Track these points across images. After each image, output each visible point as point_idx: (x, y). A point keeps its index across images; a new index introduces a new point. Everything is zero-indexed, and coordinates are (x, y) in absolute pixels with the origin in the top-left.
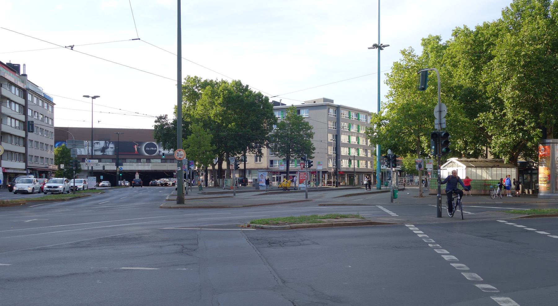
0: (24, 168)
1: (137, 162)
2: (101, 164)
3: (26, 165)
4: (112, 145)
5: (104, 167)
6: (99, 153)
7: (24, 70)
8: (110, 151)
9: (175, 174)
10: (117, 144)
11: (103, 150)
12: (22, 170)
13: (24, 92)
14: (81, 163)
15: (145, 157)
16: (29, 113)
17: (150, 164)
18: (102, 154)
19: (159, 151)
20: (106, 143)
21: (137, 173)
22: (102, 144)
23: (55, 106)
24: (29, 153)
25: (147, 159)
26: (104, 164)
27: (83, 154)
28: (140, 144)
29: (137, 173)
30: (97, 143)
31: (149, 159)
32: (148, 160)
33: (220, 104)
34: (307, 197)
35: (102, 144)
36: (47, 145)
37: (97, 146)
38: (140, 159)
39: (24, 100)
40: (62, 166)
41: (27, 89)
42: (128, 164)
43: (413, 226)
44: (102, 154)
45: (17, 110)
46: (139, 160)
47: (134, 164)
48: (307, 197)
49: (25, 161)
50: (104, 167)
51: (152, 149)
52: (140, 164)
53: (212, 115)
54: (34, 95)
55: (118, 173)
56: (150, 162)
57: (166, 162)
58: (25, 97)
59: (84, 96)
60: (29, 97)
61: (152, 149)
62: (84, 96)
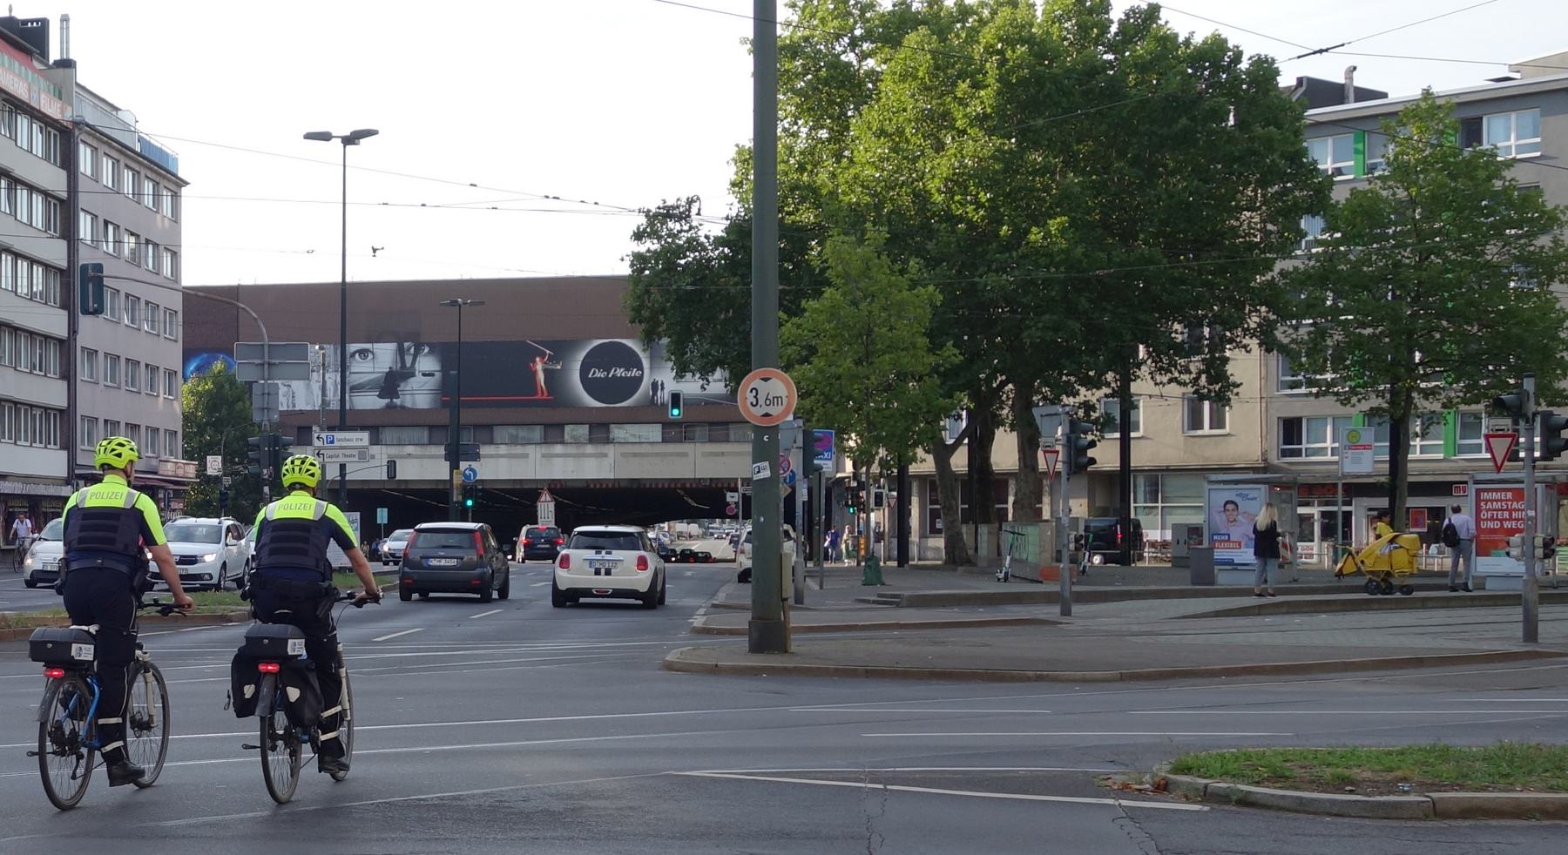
0: (63, 472)
1: (546, 441)
2: (381, 454)
5: (392, 466)
6: (370, 402)
8: (419, 393)
9: (732, 498)
10: (454, 357)
11: (390, 384)
13: (64, 139)
15: (581, 415)
17: (610, 450)
19: (654, 386)
20: (401, 352)
21: (546, 497)
22: (384, 355)
24: (83, 409)
25: (593, 427)
26: (393, 451)
28: (561, 349)
29: (546, 497)
31: (605, 426)
32: (600, 430)
33: (981, 120)
34: (1531, 634)
35: (384, 355)
36: (153, 369)
38: (561, 426)
39: (63, 174)
40: (214, 464)
41: (76, 124)
42: (503, 449)
46: (553, 432)
47: (530, 449)
48: (1531, 634)
49: (68, 445)
50: (392, 466)
51: (620, 372)
52: (559, 449)
53: (932, 185)
56: (608, 441)
58: (68, 162)
59: (309, 136)
60: (85, 156)
61: (620, 372)
62: (309, 136)
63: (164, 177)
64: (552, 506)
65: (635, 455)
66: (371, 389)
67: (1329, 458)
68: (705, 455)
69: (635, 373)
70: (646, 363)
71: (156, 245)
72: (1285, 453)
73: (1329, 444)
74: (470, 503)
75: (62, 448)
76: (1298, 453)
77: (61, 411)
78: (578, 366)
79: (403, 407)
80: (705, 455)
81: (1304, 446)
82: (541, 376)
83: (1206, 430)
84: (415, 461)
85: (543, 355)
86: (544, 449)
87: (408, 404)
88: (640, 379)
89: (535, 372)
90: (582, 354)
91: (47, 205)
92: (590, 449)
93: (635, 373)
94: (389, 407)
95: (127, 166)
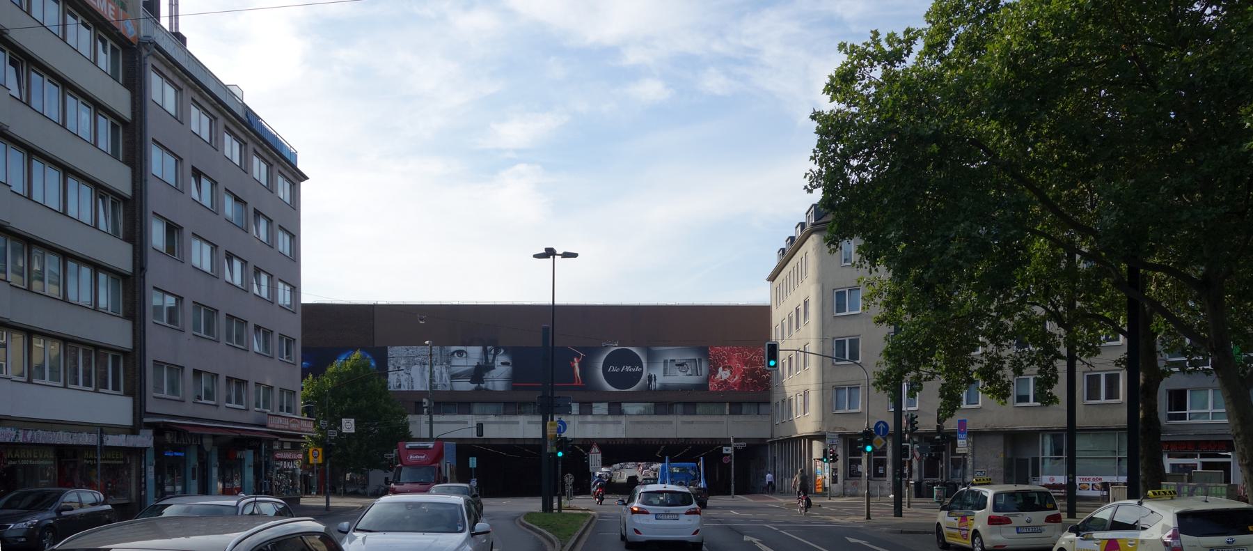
0: (127, 419)
2: (472, 420)
3: (139, 410)
4: (501, 358)
5: (480, 427)
6: (465, 385)
7: (174, 16)
8: (498, 377)
9: (1020, 501)
10: (519, 359)
11: (478, 374)
12: (117, 429)
14: (410, 418)
15: (602, 396)
16: (159, 164)
17: (622, 419)
18: (473, 386)
19: (650, 377)
20: (485, 352)
21: (595, 449)
22: (474, 354)
23: (304, 185)
26: (480, 419)
27: (418, 387)
28: (590, 353)
29: (595, 449)
30: (460, 353)
35: (474, 354)
37: (461, 364)
40: (348, 425)
43: (191, 431)
44: (473, 386)
45: (104, 142)
49: (136, 391)
50: (480, 427)
51: (628, 369)
52: (589, 418)
54: (276, 167)
55: (550, 449)
56: (621, 413)
57: (671, 413)
58: (134, 83)
59: (575, 255)
61: (628, 369)
62: (575, 255)
63: (278, 162)
64: (599, 456)
65: (638, 422)
66: (465, 377)
67: (1210, 421)
68: (684, 422)
69: (637, 369)
70: (645, 365)
71: (269, 221)
72: (1171, 417)
73: (1210, 410)
74: (560, 454)
75: (126, 394)
76: (1183, 417)
77: (125, 353)
78: (600, 366)
79: (486, 390)
80: (684, 422)
81: (1188, 412)
82: (577, 370)
83: (1103, 400)
84: (495, 426)
85: (578, 356)
86: (581, 418)
87: (490, 387)
88: (641, 373)
89: (573, 368)
90: (604, 356)
91: (114, 127)
92: (610, 418)
93: (637, 369)
94: (477, 389)
95: (231, 133)
